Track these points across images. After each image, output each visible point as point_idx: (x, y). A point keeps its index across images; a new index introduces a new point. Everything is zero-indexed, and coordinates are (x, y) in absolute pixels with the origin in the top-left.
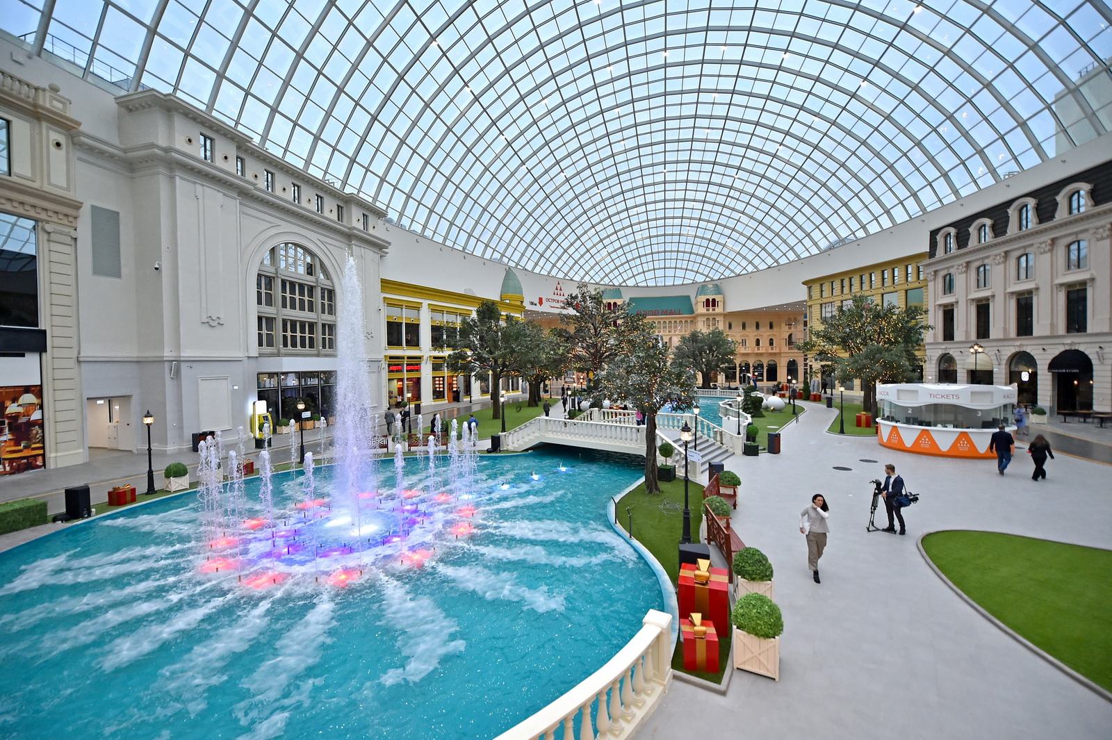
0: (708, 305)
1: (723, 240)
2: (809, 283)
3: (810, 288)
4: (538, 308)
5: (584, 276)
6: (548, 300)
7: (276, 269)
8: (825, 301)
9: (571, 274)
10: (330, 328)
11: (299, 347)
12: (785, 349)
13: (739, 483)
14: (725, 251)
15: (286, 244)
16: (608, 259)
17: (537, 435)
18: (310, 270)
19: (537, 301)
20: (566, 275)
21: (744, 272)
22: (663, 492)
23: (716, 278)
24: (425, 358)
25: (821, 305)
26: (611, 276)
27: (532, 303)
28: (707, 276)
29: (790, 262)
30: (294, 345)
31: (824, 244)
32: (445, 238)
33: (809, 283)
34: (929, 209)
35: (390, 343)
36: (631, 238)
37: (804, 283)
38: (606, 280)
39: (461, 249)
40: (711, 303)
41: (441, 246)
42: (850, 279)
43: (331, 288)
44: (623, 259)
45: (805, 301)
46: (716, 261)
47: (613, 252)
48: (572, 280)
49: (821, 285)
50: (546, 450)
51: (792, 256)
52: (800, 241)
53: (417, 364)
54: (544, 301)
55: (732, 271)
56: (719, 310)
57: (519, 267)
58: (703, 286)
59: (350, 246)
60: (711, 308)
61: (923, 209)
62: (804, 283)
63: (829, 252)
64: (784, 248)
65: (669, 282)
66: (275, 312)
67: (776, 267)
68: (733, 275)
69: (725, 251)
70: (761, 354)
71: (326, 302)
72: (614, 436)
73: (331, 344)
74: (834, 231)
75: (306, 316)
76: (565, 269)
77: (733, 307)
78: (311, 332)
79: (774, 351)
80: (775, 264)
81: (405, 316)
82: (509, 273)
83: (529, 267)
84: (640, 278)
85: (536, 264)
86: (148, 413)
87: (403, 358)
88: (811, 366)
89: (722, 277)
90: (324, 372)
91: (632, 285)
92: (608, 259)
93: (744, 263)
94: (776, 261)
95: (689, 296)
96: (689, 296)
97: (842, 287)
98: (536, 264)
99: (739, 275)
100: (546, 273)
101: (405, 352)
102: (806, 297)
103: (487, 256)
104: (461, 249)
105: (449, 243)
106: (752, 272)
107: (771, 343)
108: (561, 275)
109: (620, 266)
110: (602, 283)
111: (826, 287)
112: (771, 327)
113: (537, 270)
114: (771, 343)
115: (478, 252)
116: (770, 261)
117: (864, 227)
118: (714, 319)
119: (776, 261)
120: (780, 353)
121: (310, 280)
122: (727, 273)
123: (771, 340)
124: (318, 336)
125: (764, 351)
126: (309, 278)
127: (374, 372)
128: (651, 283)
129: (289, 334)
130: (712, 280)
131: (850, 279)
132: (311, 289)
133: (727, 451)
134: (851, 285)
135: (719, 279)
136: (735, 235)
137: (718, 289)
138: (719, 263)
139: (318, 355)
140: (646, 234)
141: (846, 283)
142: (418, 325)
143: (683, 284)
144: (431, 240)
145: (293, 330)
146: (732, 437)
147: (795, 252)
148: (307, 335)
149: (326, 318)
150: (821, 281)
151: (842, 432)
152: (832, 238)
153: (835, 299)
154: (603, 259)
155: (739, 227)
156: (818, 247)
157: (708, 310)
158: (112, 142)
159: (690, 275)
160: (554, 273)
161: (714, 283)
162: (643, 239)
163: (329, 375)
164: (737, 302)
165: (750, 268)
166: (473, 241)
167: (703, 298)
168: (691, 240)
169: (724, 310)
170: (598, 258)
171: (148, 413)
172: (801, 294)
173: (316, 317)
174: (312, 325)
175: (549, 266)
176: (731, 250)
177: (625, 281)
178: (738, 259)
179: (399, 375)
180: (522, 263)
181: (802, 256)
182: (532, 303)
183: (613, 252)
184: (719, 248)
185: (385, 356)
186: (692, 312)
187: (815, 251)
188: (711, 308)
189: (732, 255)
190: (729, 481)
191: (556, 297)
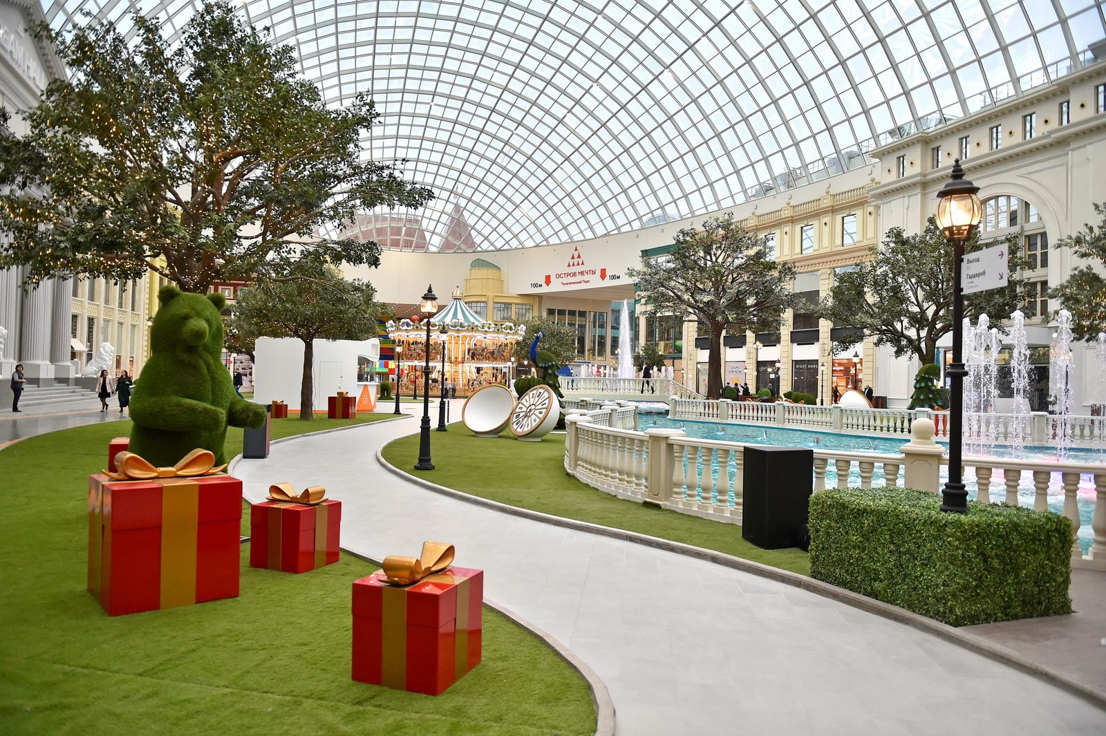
6: (559, 276)
19: (542, 281)
21: (507, 247)
34: (697, 213)
52: (887, 102)
55: (492, 244)
61: (692, 212)
68: (492, 248)
80: (545, 243)
86: (430, 290)
93: (508, 236)
99: (499, 250)
106: (516, 249)
116: (538, 238)
117: (662, 207)
119: (618, 228)
156: (593, 232)
158: (1036, 174)
165: (514, 243)
171: (430, 290)
181: (576, 239)
191: (572, 270)
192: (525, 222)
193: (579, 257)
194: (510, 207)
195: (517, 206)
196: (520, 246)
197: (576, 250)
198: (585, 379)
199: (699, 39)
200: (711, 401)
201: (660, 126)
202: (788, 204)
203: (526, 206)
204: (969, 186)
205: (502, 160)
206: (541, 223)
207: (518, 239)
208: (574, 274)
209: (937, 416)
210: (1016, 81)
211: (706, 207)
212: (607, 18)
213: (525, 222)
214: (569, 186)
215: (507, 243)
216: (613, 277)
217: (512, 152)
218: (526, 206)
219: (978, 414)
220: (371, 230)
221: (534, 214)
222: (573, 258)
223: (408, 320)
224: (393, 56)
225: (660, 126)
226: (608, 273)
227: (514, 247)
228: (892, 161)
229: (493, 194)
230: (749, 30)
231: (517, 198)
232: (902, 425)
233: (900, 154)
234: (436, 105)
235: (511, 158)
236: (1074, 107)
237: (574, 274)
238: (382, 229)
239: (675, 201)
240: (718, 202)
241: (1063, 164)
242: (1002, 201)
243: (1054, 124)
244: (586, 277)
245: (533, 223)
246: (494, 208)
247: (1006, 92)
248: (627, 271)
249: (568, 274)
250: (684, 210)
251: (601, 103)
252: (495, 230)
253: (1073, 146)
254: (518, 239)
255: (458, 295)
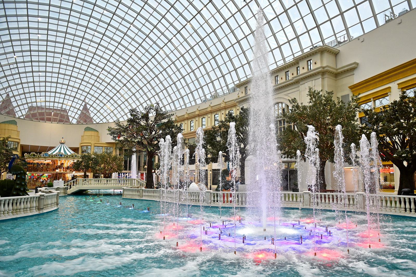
21: (101, 122)
34: (178, 109)
61: (176, 109)
93: (102, 117)
99: (98, 123)
106: (105, 123)
165: (105, 121)
192: (109, 112)
194: (102, 105)
195: (105, 105)
198: (114, 180)
199: (172, 38)
200: (402, 196)
201: (161, 73)
202: (210, 106)
203: (108, 105)
205: (97, 84)
206: (116, 112)
207: (106, 119)
209: (224, 194)
210: (284, 59)
211: (181, 107)
212: (134, 26)
213: (109, 112)
214: (127, 97)
215: (101, 120)
217: (101, 81)
218: (108, 105)
219: (273, 192)
220: (44, 113)
221: (112, 108)
223: (34, 153)
224: (90, 47)
225: (161, 73)
228: (243, 89)
230: (191, 35)
231: (105, 101)
232: (214, 199)
233: (245, 86)
234: (60, 58)
235: (101, 84)
236: (301, 69)
238: (41, 113)
239: (169, 104)
240: (185, 105)
241: (298, 91)
242: (280, 105)
243: (295, 75)
245: (112, 112)
247: (281, 63)
248: (108, 128)
250: (173, 108)
251: (137, 62)
252: (96, 114)
253: (301, 83)
254: (106, 119)
255: (63, 141)
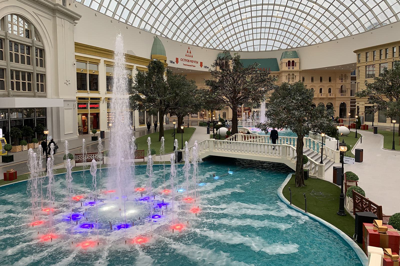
0: (289, 65)
1: (301, 21)
2: (357, 52)
3: (359, 55)
4: (175, 65)
5: (206, 43)
6: (182, 60)
7: (6, 33)
8: (368, 64)
9: (197, 42)
10: (42, 77)
11: (21, 90)
12: (339, 95)
13: (358, 179)
14: (302, 28)
15: (12, 15)
16: (223, 32)
17: (207, 150)
18: (28, 33)
19: (174, 60)
20: (194, 42)
21: (314, 43)
22: (306, 186)
23: (294, 46)
24: (102, 99)
25: (366, 66)
26: (224, 44)
27: (171, 62)
28: (289, 45)
29: (345, 37)
30: (18, 89)
31: (367, 25)
32: (114, 14)
33: (357, 52)
35: (79, 88)
36: (239, 18)
37: (355, 52)
38: (221, 47)
39: (124, 21)
40: (291, 64)
41: (112, 19)
42: (386, 49)
43: (42, 48)
44: (233, 32)
45: (355, 64)
46: (295, 35)
47: (226, 27)
48: (198, 46)
49: (367, 53)
50: (212, 161)
51: (346, 33)
53: (97, 104)
54: (179, 60)
55: (306, 42)
56: (296, 68)
57: (163, 36)
58: (286, 52)
59: (54, 17)
60: (291, 67)
62: (355, 52)
63: (371, 31)
64: (342, 28)
65: (263, 49)
66: (6, 64)
67: (335, 41)
69: (302, 28)
70: (323, 98)
71: (39, 58)
72: (263, 150)
73: (43, 88)
74: (376, 17)
75: (25, 67)
76: (194, 38)
77: (305, 67)
78: (29, 79)
79: (331, 97)
80: (335, 38)
81: (89, 69)
82: (156, 39)
83: (170, 36)
84: (243, 46)
85: (174, 34)
87: (88, 99)
88: (358, 107)
89: (299, 46)
90: (26, 109)
91: (238, 50)
92: (223, 32)
93: (314, 37)
94: (336, 36)
95: (276, 59)
96: (276, 59)
97: (381, 55)
98: (174, 34)
99: (310, 45)
100: (181, 41)
101: (88, 94)
102: (355, 61)
103: (142, 26)
104: (124, 21)
105: (117, 17)
106: (319, 43)
107: (330, 91)
108: (190, 42)
109: (230, 37)
110: (218, 48)
111: (370, 54)
112: (330, 81)
113: (174, 39)
114: (330, 91)
115: (136, 24)
116: (331, 36)
118: (293, 74)
120: (335, 98)
121: (28, 41)
122: (302, 44)
123: (330, 89)
124: (34, 82)
125: (325, 97)
126: (27, 40)
127: (71, 109)
128: (251, 49)
129: (15, 80)
130: (292, 48)
131: (386, 49)
132: (29, 48)
133: (330, 161)
134: (386, 54)
135: (297, 47)
136: (309, 18)
137: (295, 54)
138: (297, 36)
139: (34, 96)
140: (249, 15)
141: (383, 52)
142: (97, 75)
143: (272, 50)
144: (105, 14)
145: (18, 78)
146: (333, 151)
147: (349, 31)
148: (27, 82)
149: (39, 69)
150: (366, 50)
151: (394, 149)
152: (374, 21)
153: (375, 62)
154: (219, 32)
155: (313, 13)
157: (289, 68)
159: (277, 44)
160: (186, 41)
161: (293, 50)
162: (247, 19)
163: (43, 111)
164: (309, 63)
165: (318, 41)
166: (133, 16)
167: (286, 60)
168: (279, 20)
169: (300, 69)
170: (216, 30)
172: (352, 59)
173: (32, 69)
174: (30, 74)
175: (182, 36)
176: (306, 28)
177: (233, 48)
178: (310, 34)
179: (84, 111)
180: (165, 33)
181: (353, 34)
182: (171, 62)
183: (226, 27)
184: (298, 26)
185: (106, 98)
186: (278, 69)
187: (362, 30)
188: (291, 67)
189: (306, 31)
190: (352, 178)
193: (190, 53)
196: (321, 42)
197: (189, 48)
204: (287, 63)
208: (188, 61)
216: (206, 67)
222: (188, 52)
226: (203, 65)
227: (318, 43)
229: (293, 11)
237: (188, 61)
244: (194, 64)
246: (264, 25)
249: (186, 60)
